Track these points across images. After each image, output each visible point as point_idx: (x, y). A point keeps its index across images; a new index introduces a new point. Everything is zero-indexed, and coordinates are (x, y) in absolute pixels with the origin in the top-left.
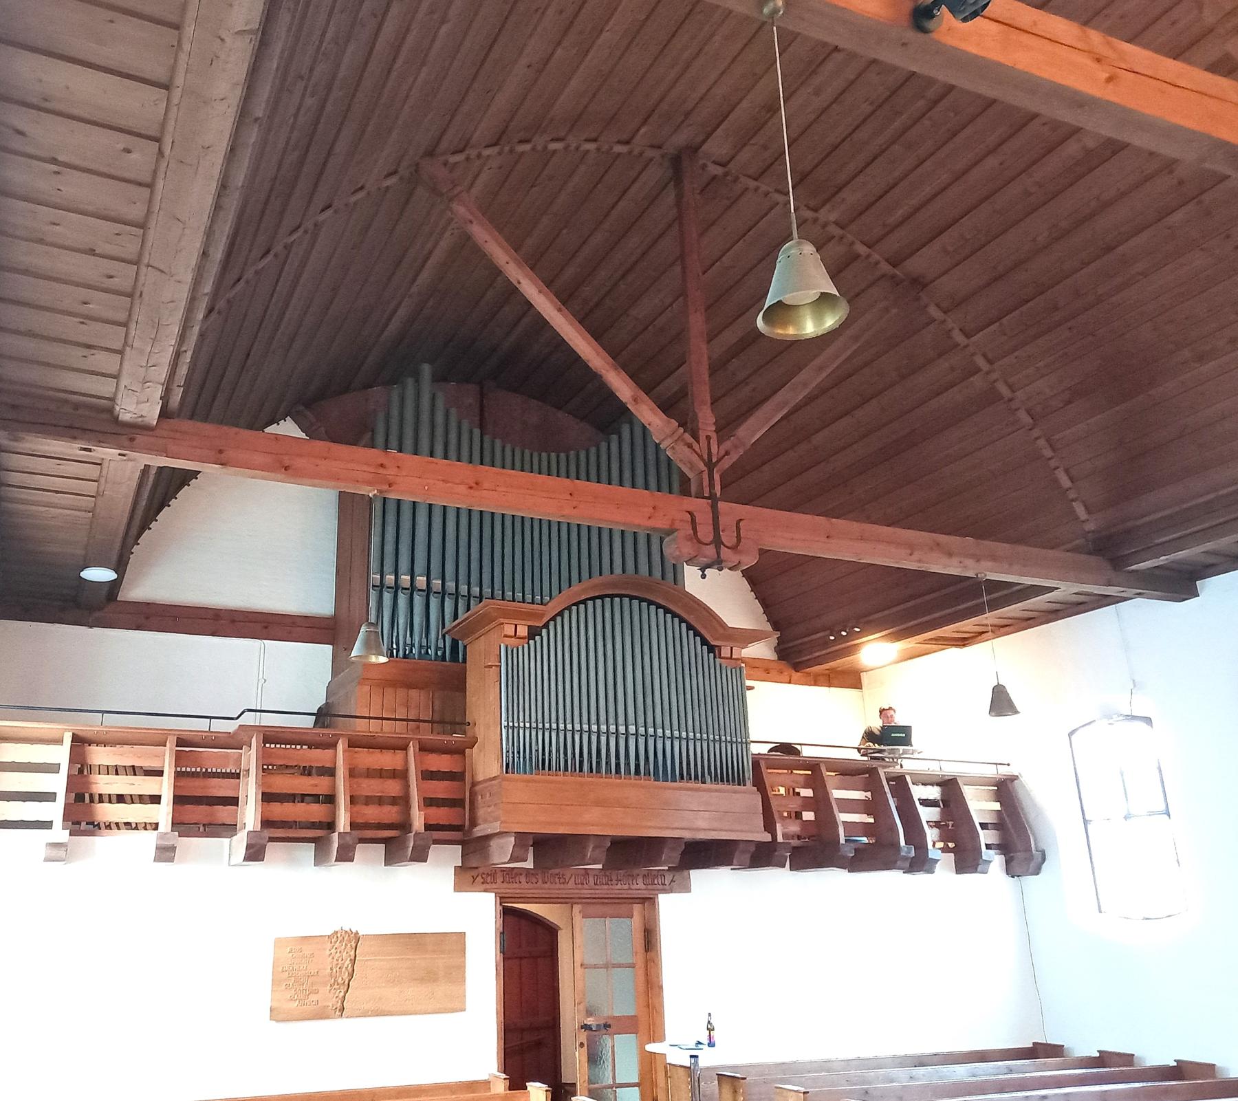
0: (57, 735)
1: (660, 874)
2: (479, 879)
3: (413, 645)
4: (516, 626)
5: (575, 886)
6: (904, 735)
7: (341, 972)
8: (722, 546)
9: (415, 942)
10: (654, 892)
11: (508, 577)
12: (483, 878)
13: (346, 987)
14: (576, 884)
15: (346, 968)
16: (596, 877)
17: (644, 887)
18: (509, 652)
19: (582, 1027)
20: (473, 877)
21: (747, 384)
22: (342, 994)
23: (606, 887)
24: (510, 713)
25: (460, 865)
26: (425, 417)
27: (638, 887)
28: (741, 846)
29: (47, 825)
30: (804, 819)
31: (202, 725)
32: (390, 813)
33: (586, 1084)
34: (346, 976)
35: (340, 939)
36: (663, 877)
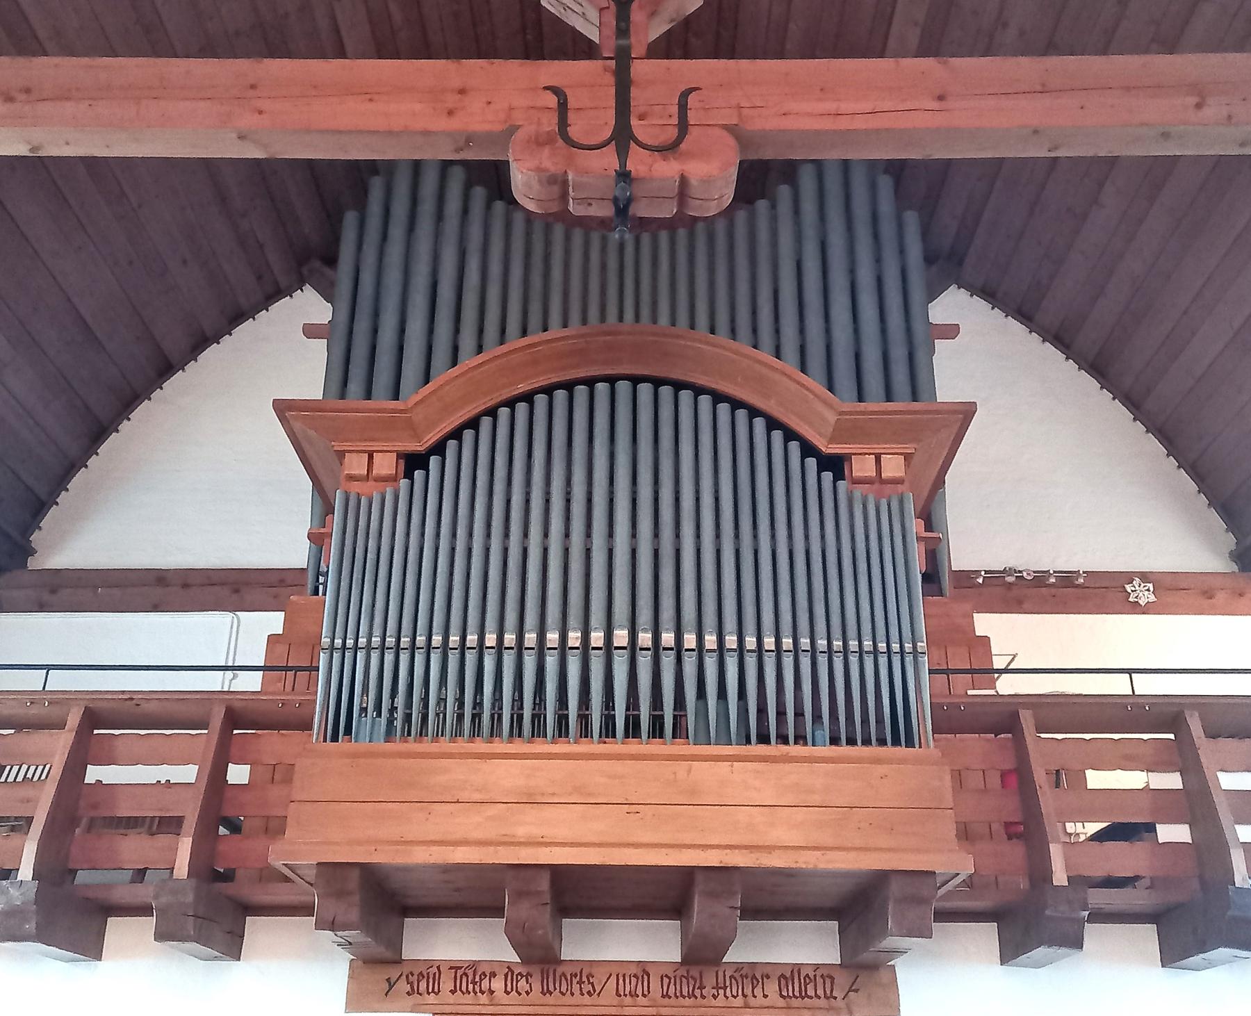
1: (819, 973)
2: (403, 986)
4: (371, 457)
5: (616, 1000)
11: (862, 566)
16: (666, 981)
17: (781, 1002)
18: (352, 504)
20: (388, 980)
21: (1005, 25)
23: (687, 1001)
36: (828, 981)
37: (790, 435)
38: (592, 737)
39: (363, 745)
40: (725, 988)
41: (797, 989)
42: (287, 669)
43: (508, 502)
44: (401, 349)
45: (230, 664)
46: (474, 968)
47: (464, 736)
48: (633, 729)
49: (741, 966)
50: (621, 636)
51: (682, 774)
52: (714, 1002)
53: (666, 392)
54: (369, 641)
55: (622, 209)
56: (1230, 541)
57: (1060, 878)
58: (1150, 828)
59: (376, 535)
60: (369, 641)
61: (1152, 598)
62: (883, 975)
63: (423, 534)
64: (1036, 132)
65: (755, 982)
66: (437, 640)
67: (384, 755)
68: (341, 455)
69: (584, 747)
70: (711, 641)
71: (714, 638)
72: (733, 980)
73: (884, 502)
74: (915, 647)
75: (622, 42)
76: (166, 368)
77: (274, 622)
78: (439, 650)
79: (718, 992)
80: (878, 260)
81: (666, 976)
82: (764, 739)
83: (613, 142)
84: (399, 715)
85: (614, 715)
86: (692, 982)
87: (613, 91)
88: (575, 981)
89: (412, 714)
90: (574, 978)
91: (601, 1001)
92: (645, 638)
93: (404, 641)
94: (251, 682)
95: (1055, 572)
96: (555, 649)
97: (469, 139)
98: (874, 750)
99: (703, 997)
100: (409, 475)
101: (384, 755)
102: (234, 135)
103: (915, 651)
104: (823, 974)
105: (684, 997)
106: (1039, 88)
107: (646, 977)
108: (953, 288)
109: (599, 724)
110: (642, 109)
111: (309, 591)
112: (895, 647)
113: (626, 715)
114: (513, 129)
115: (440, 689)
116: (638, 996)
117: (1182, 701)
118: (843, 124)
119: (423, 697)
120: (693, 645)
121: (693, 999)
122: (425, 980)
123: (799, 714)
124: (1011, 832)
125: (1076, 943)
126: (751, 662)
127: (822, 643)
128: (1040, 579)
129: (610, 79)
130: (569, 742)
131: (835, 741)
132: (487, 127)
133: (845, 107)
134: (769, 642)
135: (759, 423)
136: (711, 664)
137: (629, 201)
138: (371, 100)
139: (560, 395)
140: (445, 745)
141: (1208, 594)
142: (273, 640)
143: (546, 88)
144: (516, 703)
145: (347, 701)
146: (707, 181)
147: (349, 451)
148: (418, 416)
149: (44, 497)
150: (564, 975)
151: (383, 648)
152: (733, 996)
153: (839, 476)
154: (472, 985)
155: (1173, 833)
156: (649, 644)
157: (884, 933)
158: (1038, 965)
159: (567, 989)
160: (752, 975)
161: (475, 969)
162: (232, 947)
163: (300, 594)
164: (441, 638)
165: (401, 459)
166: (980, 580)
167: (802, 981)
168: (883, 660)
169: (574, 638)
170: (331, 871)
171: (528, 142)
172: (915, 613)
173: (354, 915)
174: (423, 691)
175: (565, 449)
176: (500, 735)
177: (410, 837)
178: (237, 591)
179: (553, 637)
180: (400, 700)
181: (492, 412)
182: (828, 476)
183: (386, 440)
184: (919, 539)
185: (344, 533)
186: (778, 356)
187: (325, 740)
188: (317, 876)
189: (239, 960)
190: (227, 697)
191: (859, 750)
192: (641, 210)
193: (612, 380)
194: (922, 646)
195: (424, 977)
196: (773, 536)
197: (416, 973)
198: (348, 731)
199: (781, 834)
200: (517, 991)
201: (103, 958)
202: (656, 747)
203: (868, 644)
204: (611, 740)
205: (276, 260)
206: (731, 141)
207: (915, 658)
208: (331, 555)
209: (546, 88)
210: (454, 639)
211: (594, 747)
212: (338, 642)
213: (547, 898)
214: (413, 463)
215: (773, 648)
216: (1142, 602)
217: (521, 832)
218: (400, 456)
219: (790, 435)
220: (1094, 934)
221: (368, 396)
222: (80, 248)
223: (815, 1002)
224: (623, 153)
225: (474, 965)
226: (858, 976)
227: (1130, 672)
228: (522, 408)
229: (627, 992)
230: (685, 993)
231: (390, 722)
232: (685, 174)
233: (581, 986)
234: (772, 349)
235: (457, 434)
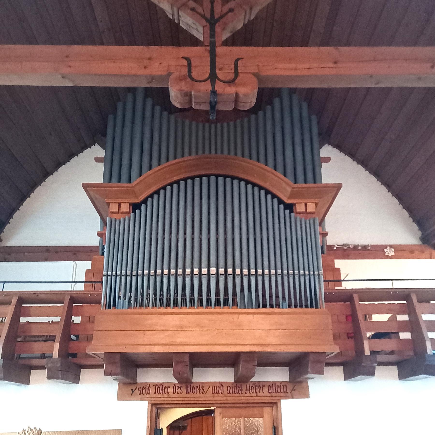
1: (282, 384)
4: (120, 205)
5: (212, 395)
10: (277, 398)
11: (300, 244)
14: (212, 393)
17: (269, 395)
20: (132, 390)
23: (238, 395)
24: (110, 265)
25: (289, 381)
27: (264, 395)
28: (311, 357)
30: (401, 338)
38: (203, 306)
39: (120, 310)
40: (249, 390)
41: (274, 390)
42: (92, 282)
43: (171, 222)
44: (131, 166)
45: (74, 281)
46: (162, 385)
47: (157, 306)
48: (218, 303)
49: (255, 383)
50: (213, 270)
51: (236, 319)
53: (228, 180)
54: (121, 272)
55: (213, 106)
56: (419, 234)
57: (367, 352)
58: (397, 333)
59: (123, 234)
60: (121, 272)
61: (393, 254)
62: (304, 384)
63: (140, 233)
64: (371, 76)
65: (260, 388)
66: (146, 272)
67: (127, 314)
68: (108, 204)
69: (200, 310)
70: (245, 271)
71: (247, 270)
72: (252, 388)
73: (308, 221)
74: (319, 272)
75: (212, 39)
76: (46, 174)
77: (87, 265)
78: (147, 276)
79: (247, 391)
80: (302, 134)
81: (229, 387)
82: (264, 306)
83: (209, 80)
84: (133, 299)
85: (211, 298)
86: (238, 388)
87: (209, 59)
88: (197, 389)
89: (137, 298)
90: (197, 388)
91: (206, 395)
92: (222, 271)
93: (134, 273)
94: (80, 287)
95: (361, 245)
96: (189, 275)
97: (153, 78)
98: (304, 310)
99: (242, 393)
100: (134, 211)
101: (127, 314)
102: (60, 76)
103: (319, 275)
104: (283, 385)
105: (235, 393)
106: (372, 59)
107: (222, 387)
109: (205, 302)
110: (220, 66)
111: (100, 254)
112: (312, 273)
113: (215, 298)
114: (170, 74)
115: (148, 289)
116: (219, 393)
117: (410, 290)
118: (298, 73)
119: (141, 292)
120: (239, 273)
121: (238, 394)
122: (145, 389)
123: (277, 297)
124: (349, 336)
125: (372, 374)
126: (260, 279)
127: (285, 272)
128: (356, 248)
129: (207, 54)
130: (195, 308)
131: (290, 306)
132: (160, 73)
133: (300, 66)
134: (266, 272)
135: (263, 192)
136: (245, 279)
137: (216, 103)
138: (114, 62)
140: (150, 310)
141: (412, 252)
142: (87, 271)
143: (183, 58)
144: (175, 295)
145: (113, 296)
146: (245, 95)
147: (112, 203)
148: (137, 189)
150: (194, 387)
151: (126, 275)
152: (252, 393)
153: (291, 211)
154: (161, 391)
155: (405, 335)
156: (223, 273)
157: (307, 373)
158: (358, 381)
159: (195, 392)
160: (259, 386)
161: (163, 385)
162: (76, 379)
163: (96, 255)
164: (147, 271)
165: (131, 205)
166: (335, 248)
167: (276, 387)
168: (307, 278)
169: (196, 271)
170: (109, 356)
171: (176, 79)
172: (319, 261)
173: (118, 370)
174: (141, 290)
175: (191, 202)
176: (170, 306)
177: (137, 343)
178: (75, 254)
179: (188, 271)
180: (133, 294)
181: (164, 188)
182: (287, 211)
183: (126, 198)
184: (320, 234)
185: (111, 233)
187: (106, 309)
188: (104, 357)
189: (79, 384)
190: (71, 293)
191: (298, 310)
192: (221, 107)
193: (208, 176)
194: (321, 272)
195: (144, 389)
196: (261, 233)
197: (142, 387)
198: (114, 305)
199: (272, 340)
200: (177, 393)
201: (30, 384)
202: (226, 310)
203: (302, 272)
204: (210, 307)
206: (255, 80)
208: (106, 242)
210: (152, 272)
211: (204, 310)
212: (110, 273)
213: (188, 363)
214: (135, 207)
215: (268, 274)
216: (390, 255)
217: (178, 340)
218: (130, 204)
219: (274, 196)
220: (379, 370)
221: (119, 182)
222: (262, 324)
223: (281, 394)
224: (213, 84)
225: (162, 384)
226: (295, 385)
227: (392, 280)
228: (175, 186)
229: (216, 392)
231: (130, 302)
232: (238, 92)
233: (199, 391)
235: (151, 196)
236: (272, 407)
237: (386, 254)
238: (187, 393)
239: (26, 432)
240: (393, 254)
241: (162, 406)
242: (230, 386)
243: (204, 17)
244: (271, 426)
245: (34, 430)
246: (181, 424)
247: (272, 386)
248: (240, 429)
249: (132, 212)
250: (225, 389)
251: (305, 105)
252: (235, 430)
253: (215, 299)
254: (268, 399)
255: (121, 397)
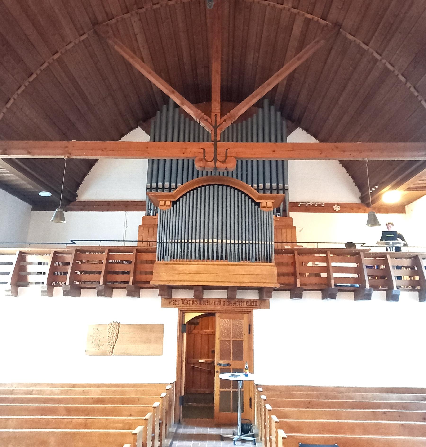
0: (48, 252)
3: (151, 209)
4: (165, 201)
5: (214, 306)
6: (393, 235)
7: (112, 338)
8: (217, 161)
9: (142, 327)
10: (252, 309)
12: (173, 302)
13: (114, 344)
14: (215, 305)
15: (115, 337)
17: (247, 306)
19: (218, 365)
20: (169, 302)
22: (113, 346)
23: (229, 306)
26: (170, 120)
27: (244, 306)
29: (6, 283)
31: (97, 244)
32: (291, 279)
33: (219, 388)
34: (114, 340)
35: (113, 325)
37: (250, 198)
52: (234, 306)
56: (359, 194)
57: (299, 285)
99: (231, 305)
100: (173, 206)
104: (255, 301)
108: (298, 128)
117: (327, 249)
126: (240, 245)
139: (203, 188)
141: (352, 208)
143: (201, 148)
149: (78, 181)
166: (299, 205)
168: (266, 245)
169: (206, 241)
178: (126, 207)
181: (189, 192)
182: (257, 206)
186: (247, 183)
194: (273, 243)
205: (132, 122)
207: (272, 245)
209: (201, 148)
212: (160, 241)
214: (174, 203)
216: (337, 210)
217: (196, 279)
223: (253, 306)
225: (186, 299)
228: (195, 191)
230: (228, 304)
234: (246, 182)
235: (182, 197)
236: (249, 313)
237: (335, 209)
238: (200, 304)
239: (112, 324)
240: (339, 209)
241: (186, 311)
242: (225, 301)
243: (211, 124)
244: (248, 324)
245: (116, 323)
246: (195, 321)
247: (248, 301)
248: (230, 326)
249: (172, 206)
250: (222, 303)
251: (279, 113)
252: (227, 326)
253: (216, 255)
254: (246, 309)
255: (163, 305)
